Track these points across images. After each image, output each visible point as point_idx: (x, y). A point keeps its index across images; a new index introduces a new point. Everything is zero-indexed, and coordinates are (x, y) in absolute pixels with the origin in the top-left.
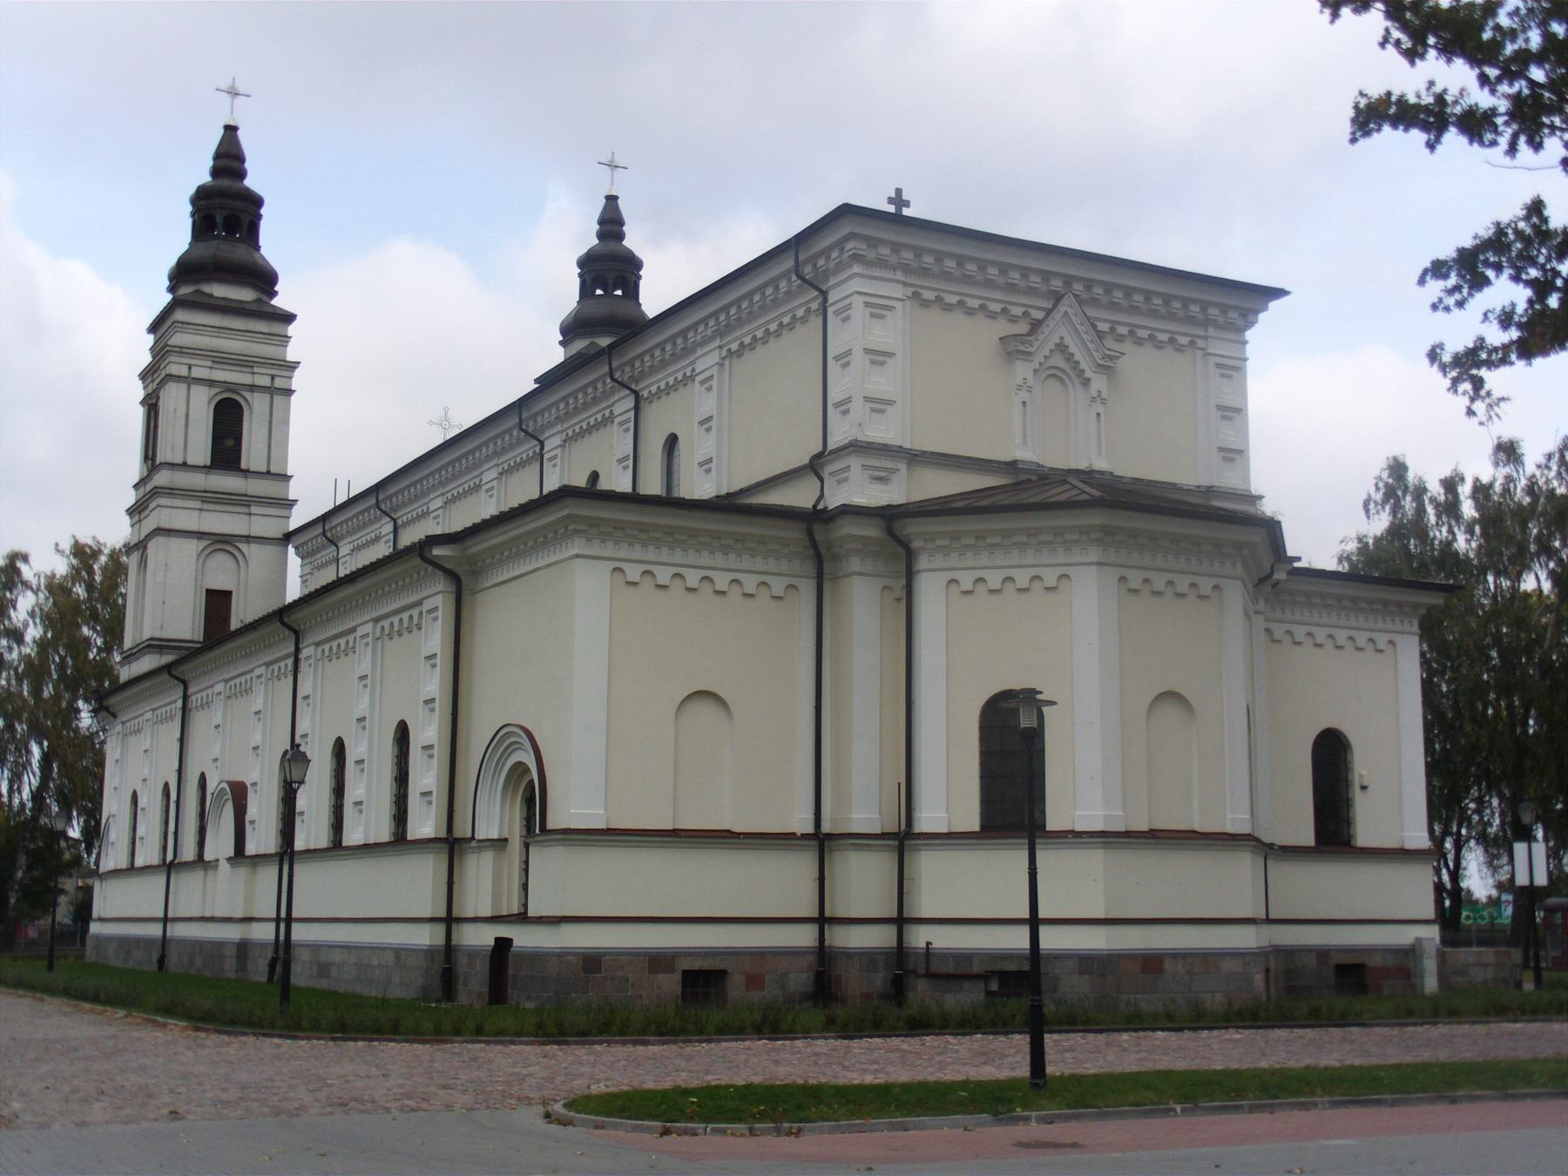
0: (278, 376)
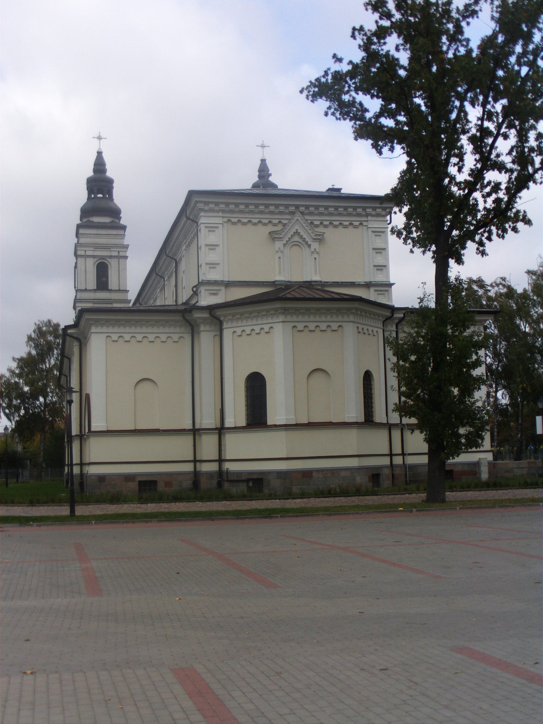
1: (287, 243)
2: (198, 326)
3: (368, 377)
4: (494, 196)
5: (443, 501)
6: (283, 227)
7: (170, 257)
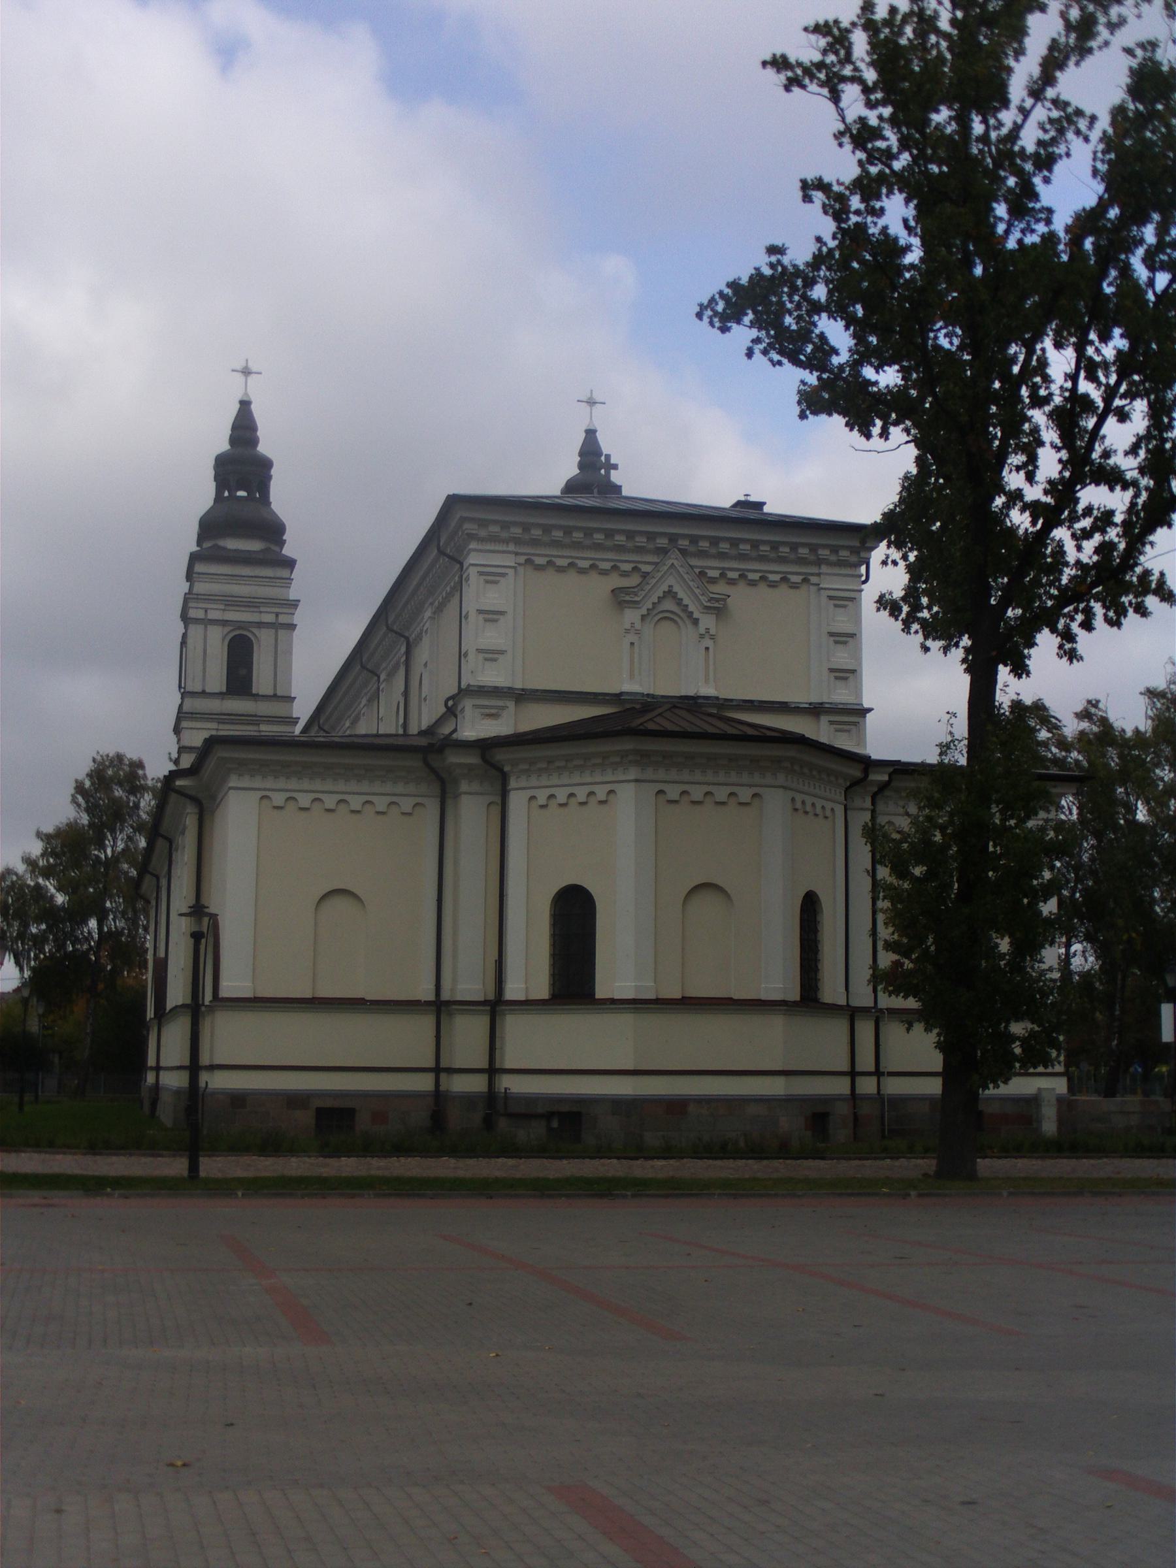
0: (281, 613)
1: (648, 614)
3: (810, 905)
4: (1097, 538)
5: (972, 1176)
6: (641, 580)
7: (396, 633)
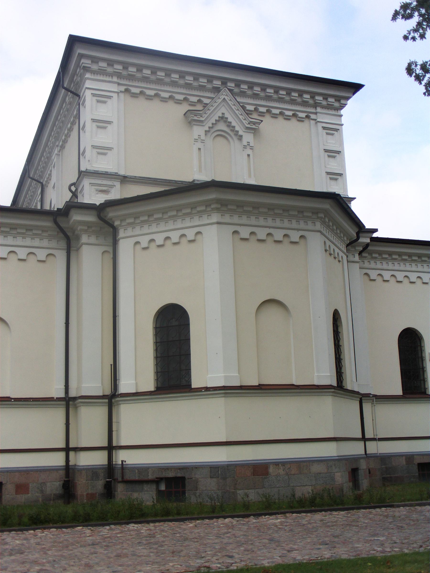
2: (78, 238)
